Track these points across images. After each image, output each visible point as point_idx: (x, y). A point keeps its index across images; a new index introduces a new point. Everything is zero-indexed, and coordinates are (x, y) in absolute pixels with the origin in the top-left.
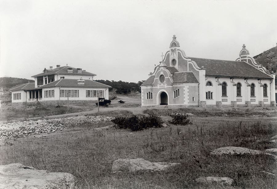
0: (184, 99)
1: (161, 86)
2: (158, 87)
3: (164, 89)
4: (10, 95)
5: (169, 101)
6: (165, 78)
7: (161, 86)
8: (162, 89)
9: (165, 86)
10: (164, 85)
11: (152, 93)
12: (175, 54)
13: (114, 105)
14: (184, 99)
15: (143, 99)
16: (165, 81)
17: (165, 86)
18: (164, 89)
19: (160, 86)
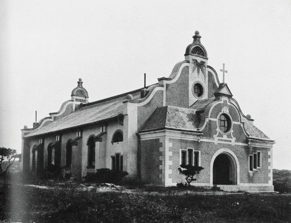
0: (269, 167)
1: (222, 140)
2: (216, 140)
3: (230, 147)
4: (80, 150)
5: (254, 159)
6: (233, 123)
7: (222, 140)
8: (224, 146)
9: (230, 141)
10: (230, 139)
11: (197, 154)
12: (200, 70)
13: (141, 101)
14: (269, 167)
15: (170, 175)
16: (232, 131)
17: (230, 141)
18: (230, 147)
19: (219, 140)
